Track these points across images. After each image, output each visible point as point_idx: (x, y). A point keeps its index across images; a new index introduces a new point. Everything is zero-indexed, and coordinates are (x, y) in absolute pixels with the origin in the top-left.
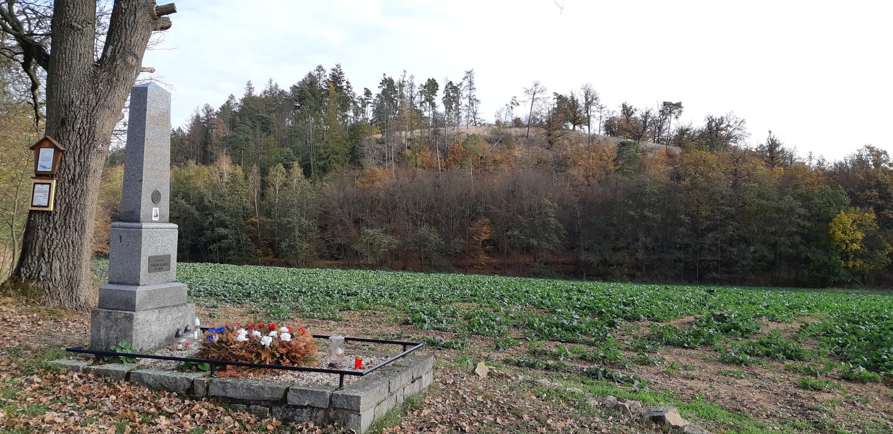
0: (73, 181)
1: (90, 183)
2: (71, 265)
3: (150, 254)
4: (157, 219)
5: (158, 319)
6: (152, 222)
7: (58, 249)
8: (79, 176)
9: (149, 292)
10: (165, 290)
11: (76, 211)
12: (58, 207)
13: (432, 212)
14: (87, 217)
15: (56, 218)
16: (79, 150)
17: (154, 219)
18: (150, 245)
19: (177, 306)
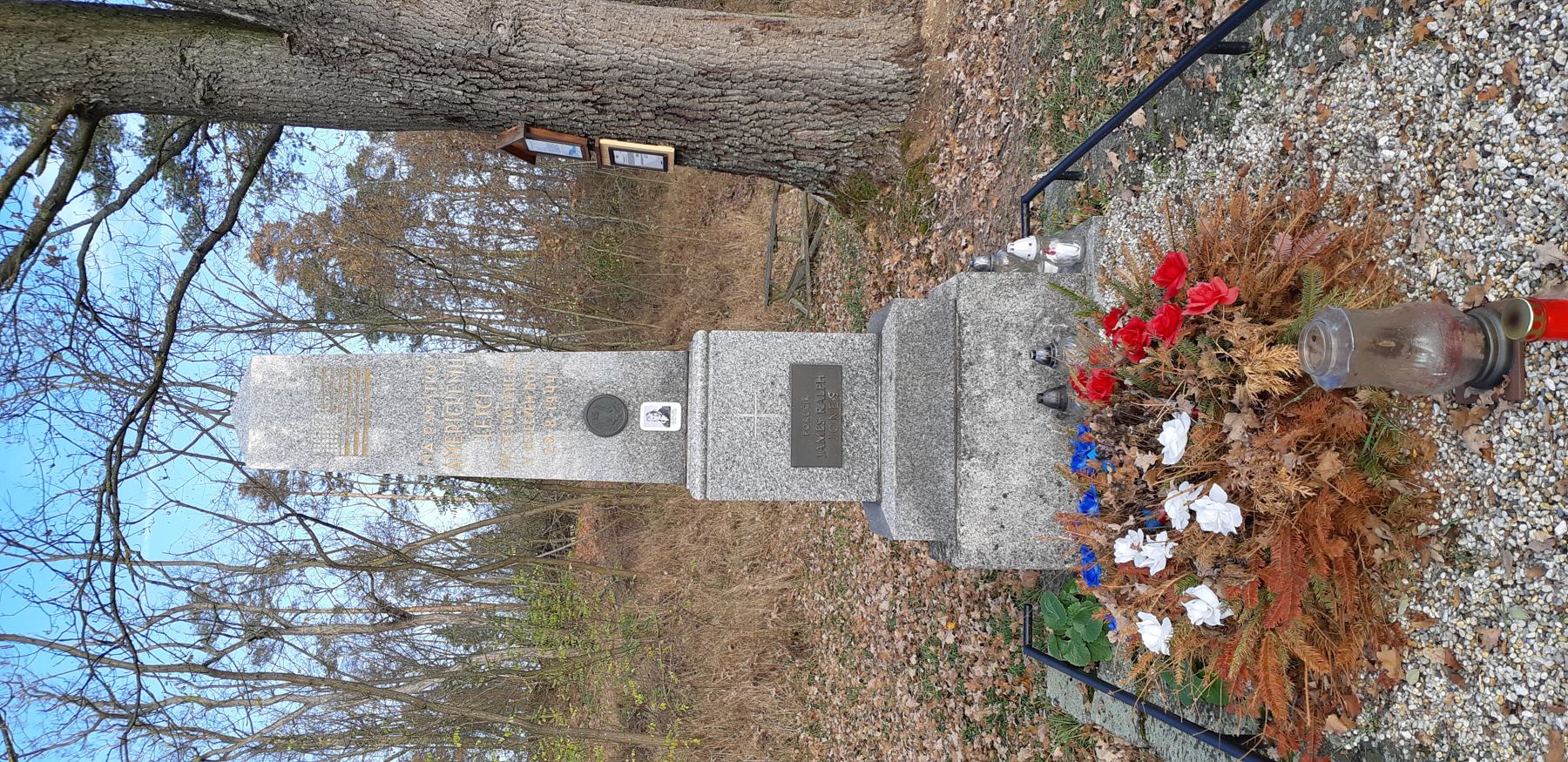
0: (600, 105)
1: (601, 60)
2: (804, 105)
3: (785, 461)
4: (676, 408)
5: (991, 460)
6: (684, 431)
7: (766, 135)
8: (585, 89)
9: (904, 480)
10: (902, 405)
11: (673, 95)
12: (664, 133)
13: (229, 26)
14: (687, 60)
15: (690, 137)
16: (520, 93)
17: (676, 426)
18: (757, 464)
19: (959, 364)
